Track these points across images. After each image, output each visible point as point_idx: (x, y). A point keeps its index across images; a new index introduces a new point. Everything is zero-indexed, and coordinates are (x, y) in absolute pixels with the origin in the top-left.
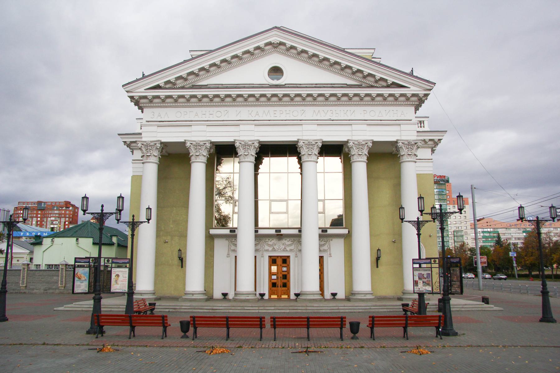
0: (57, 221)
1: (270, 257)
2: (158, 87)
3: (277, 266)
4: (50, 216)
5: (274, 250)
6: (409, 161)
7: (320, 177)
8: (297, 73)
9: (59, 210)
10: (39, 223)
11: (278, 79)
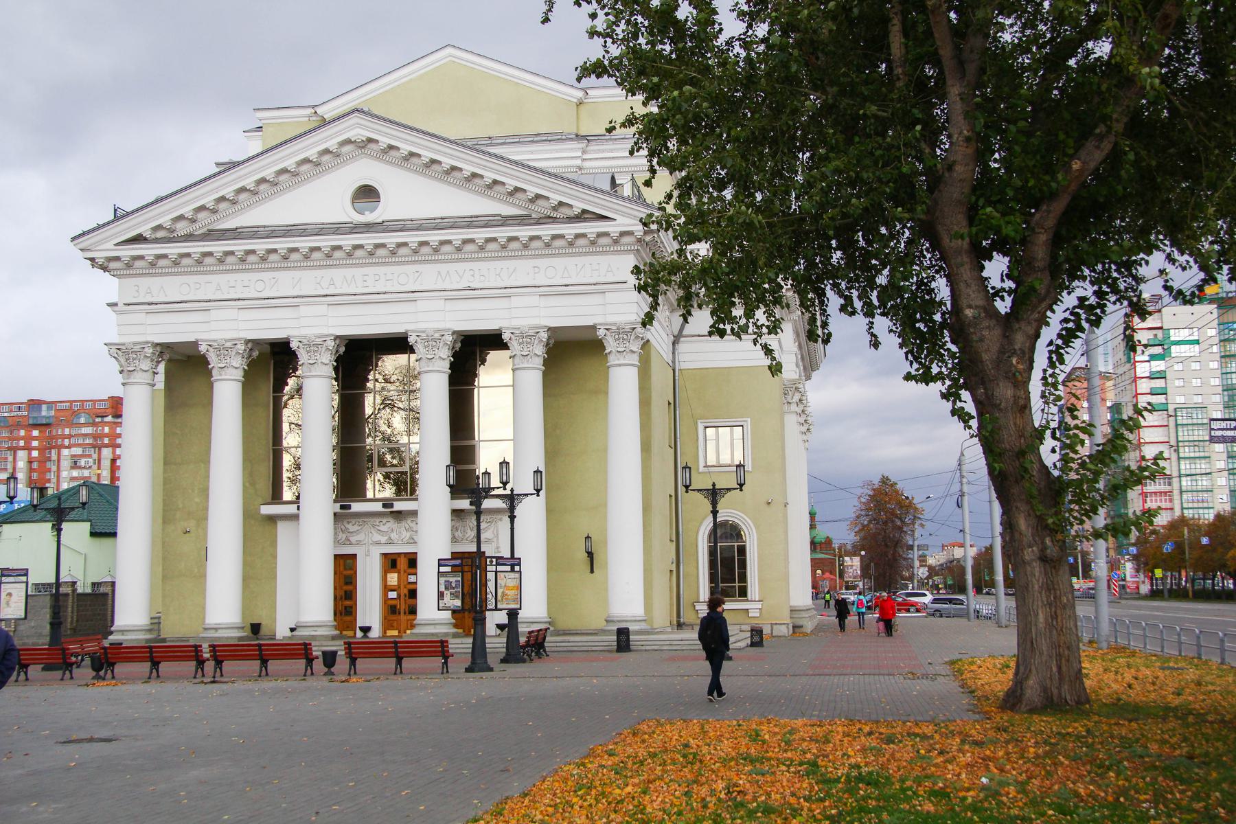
0: (90, 456)
1: (385, 555)
2: (138, 239)
3: (399, 573)
4: (66, 442)
5: (390, 542)
6: (619, 365)
7: (476, 391)
8: (407, 196)
9: (94, 424)
10: (35, 466)
11: (372, 211)
